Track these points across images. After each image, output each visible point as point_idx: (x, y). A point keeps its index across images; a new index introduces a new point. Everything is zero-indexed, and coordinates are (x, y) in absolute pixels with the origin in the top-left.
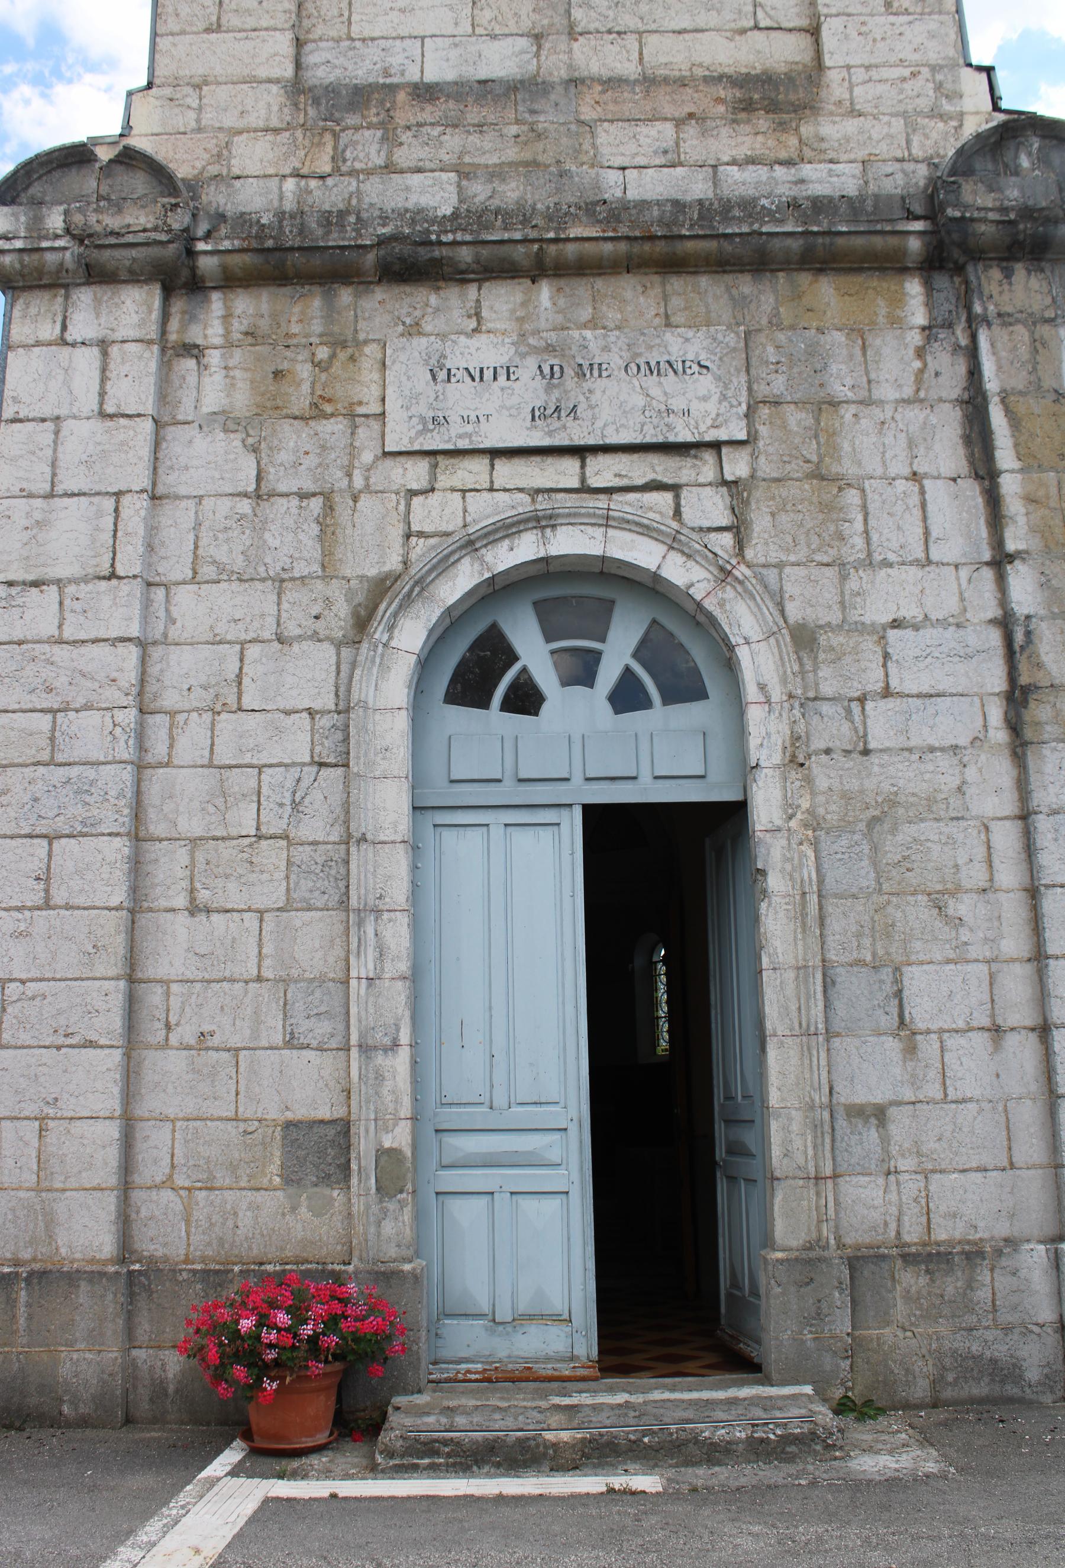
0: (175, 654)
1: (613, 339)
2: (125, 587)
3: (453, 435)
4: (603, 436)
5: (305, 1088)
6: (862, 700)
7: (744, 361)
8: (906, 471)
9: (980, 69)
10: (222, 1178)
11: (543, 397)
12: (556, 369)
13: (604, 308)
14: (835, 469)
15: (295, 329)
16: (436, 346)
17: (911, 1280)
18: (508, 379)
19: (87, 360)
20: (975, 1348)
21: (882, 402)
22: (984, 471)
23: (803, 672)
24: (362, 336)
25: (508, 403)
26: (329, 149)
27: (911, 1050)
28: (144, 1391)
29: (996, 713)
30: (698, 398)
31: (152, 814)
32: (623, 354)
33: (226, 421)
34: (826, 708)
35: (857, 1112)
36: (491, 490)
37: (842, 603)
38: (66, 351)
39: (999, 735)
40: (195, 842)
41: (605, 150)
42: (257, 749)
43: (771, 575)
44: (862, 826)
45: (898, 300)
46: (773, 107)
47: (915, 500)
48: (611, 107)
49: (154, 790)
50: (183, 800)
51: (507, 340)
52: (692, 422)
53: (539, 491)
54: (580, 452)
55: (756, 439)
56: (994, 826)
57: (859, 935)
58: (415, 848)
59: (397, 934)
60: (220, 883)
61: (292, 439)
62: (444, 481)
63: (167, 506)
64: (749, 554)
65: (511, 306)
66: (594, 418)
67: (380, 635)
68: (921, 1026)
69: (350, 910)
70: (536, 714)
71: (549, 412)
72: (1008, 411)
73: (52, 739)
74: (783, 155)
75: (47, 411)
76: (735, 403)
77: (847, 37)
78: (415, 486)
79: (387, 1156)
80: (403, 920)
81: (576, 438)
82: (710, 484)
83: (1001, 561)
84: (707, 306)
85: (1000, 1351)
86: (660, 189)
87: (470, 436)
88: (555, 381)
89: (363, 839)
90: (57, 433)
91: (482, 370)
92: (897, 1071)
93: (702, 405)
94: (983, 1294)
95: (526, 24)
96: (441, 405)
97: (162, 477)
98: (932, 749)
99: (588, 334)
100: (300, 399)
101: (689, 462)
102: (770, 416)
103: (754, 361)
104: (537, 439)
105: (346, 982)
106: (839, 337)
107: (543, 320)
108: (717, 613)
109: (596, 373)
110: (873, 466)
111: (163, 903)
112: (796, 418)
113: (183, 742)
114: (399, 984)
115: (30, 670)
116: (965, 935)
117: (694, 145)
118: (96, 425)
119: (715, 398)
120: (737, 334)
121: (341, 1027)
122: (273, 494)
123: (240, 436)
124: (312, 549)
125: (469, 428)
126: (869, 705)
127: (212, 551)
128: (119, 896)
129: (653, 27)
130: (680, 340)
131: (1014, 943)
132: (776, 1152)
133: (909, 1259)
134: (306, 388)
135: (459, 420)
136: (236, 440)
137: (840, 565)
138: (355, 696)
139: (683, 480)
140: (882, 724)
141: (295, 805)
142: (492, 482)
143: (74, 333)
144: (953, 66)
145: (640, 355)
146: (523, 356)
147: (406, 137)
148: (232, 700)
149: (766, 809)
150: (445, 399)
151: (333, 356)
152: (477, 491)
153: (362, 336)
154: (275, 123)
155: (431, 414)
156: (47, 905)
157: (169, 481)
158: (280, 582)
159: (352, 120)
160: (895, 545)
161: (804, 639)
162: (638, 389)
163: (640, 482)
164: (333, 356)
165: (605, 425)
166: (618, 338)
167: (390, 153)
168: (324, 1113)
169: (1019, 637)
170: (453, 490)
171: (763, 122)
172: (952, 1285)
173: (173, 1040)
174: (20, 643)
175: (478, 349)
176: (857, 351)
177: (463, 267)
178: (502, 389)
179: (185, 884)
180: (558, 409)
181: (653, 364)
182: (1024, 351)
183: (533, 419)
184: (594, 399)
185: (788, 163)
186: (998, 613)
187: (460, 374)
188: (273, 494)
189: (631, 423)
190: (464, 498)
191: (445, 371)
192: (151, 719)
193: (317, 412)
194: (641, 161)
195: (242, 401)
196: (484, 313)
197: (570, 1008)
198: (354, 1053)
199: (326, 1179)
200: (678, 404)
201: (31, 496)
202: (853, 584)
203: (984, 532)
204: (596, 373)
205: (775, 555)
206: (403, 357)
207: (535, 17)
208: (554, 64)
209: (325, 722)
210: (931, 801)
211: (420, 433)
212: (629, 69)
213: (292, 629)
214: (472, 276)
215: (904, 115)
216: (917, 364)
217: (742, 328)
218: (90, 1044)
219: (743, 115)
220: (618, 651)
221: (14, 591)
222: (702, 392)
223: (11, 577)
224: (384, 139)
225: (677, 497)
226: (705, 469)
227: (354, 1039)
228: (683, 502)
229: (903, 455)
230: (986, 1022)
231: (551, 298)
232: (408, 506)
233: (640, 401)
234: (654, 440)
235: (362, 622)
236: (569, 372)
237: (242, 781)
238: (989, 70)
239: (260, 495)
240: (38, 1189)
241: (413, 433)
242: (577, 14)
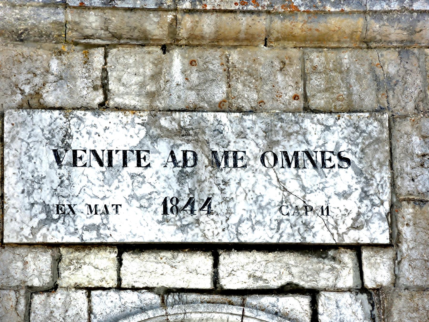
1: (248, 124)
3: (79, 227)
4: (238, 234)
7: (387, 154)
11: (176, 187)
12: (189, 155)
13: (240, 86)
16: (60, 123)
18: (139, 165)
25: (139, 192)
30: (337, 195)
32: (260, 141)
36: (119, 288)
51: (137, 120)
52: (331, 221)
53: (169, 291)
54: (214, 250)
55: (399, 242)
62: (68, 277)
65: (139, 79)
66: (229, 212)
71: (182, 204)
76: (377, 202)
78: (36, 283)
81: (209, 234)
82: (350, 290)
84: (349, 87)
87: (97, 228)
88: (189, 170)
91: (110, 153)
96: (66, 192)
99: (222, 116)
101: (327, 264)
102: (415, 215)
103: (398, 152)
104: (170, 234)
107: (174, 97)
109: (231, 162)
119: (356, 195)
120: (380, 121)
125: (97, 219)
130: (320, 128)
135: (86, 210)
139: (321, 284)
142: (119, 280)
145: (278, 143)
146: (154, 139)
150: (71, 184)
152: (103, 289)
155: (55, 201)
162: (275, 182)
163: (275, 284)
165: (241, 221)
166: (254, 123)
170: (78, 287)
175: (106, 129)
177: (89, 32)
178: (132, 176)
180: (191, 202)
181: (291, 154)
183: (165, 212)
184: (230, 190)
187: (86, 157)
189: (267, 220)
190: (89, 296)
191: (70, 153)
196: (112, 86)
200: (316, 200)
204: (231, 162)
206: (23, 134)
211: (43, 223)
214: (99, 42)
217: (386, 116)
222: (342, 188)
225: (314, 304)
226: (344, 273)
228: (320, 309)
231: (183, 72)
232: (29, 305)
233: (274, 195)
234: (291, 240)
236: (203, 160)
241: (35, 223)
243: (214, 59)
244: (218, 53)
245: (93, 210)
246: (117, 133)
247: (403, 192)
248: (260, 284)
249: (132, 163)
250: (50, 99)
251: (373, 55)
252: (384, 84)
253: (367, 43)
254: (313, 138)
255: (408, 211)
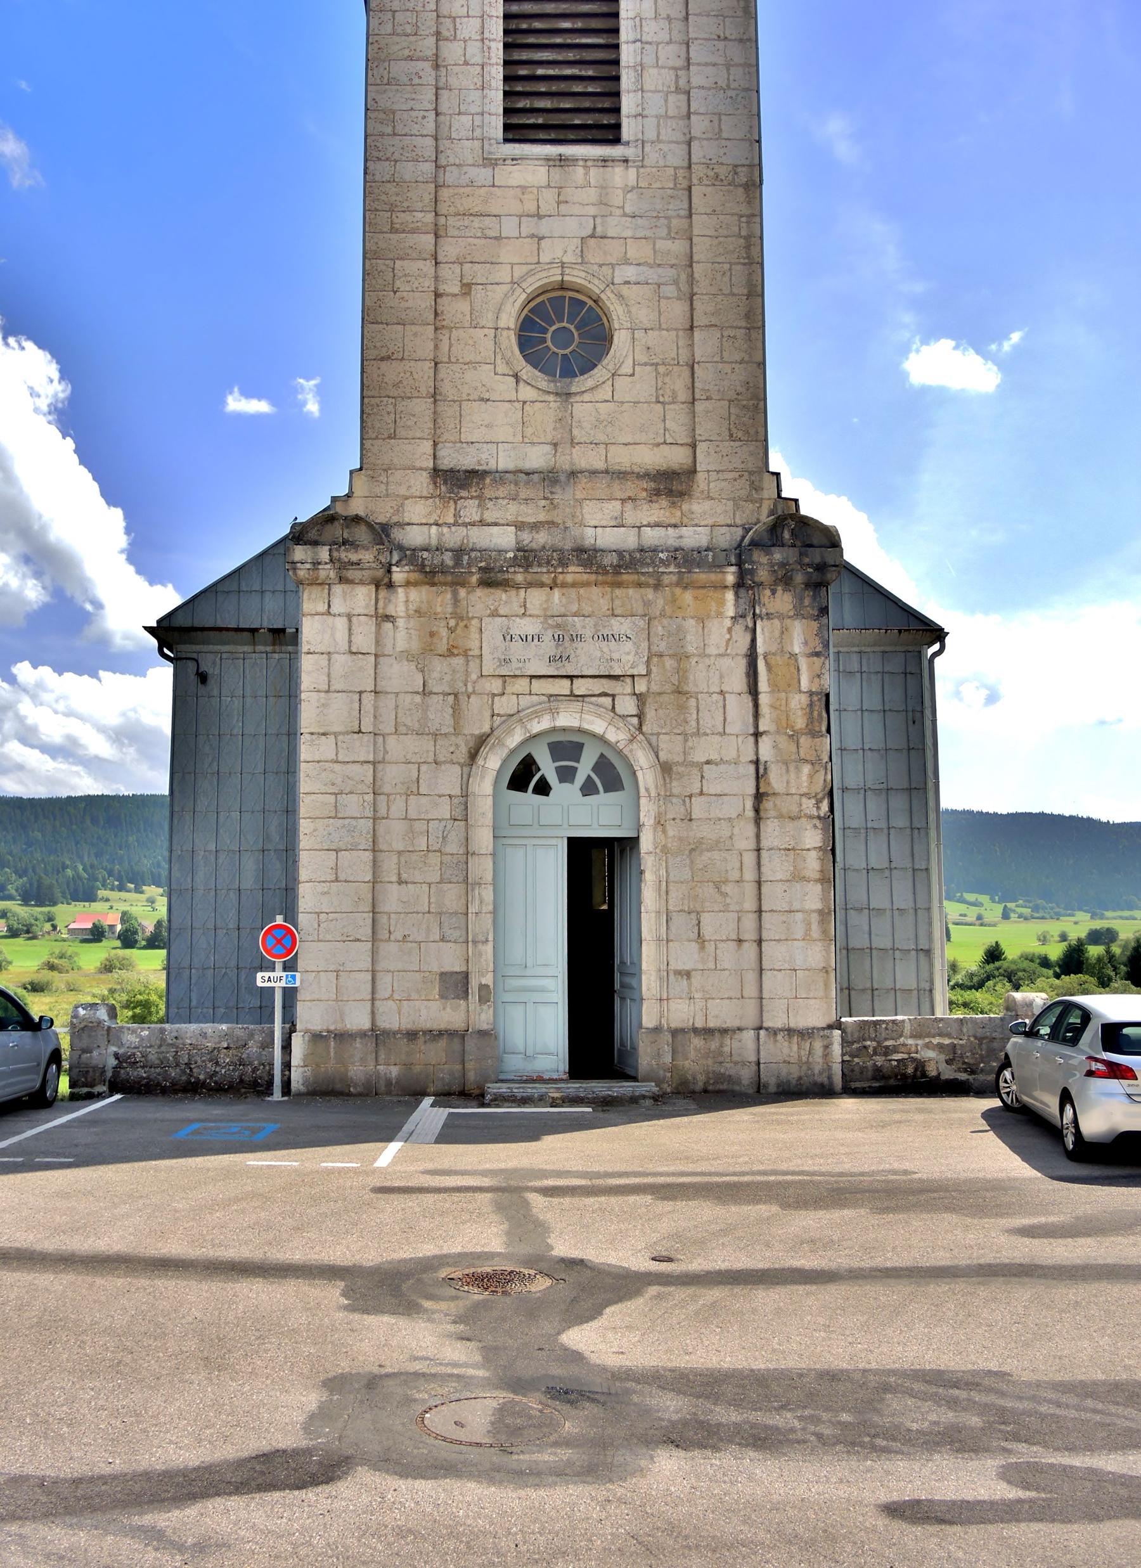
0: (389, 767)
2: (366, 738)
5: (450, 959)
6: (690, 796)
8: (718, 690)
9: (773, 473)
10: (414, 996)
14: (686, 688)
15: (439, 610)
17: (697, 1042)
19: (341, 624)
20: (722, 1071)
21: (710, 656)
22: (753, 691)
23: (665, 784)
24: (470, 615)
26: (452, 510)
27: (702, 948)
28: (382, 1083)
29: (749, 804)
31: (380, 840)
33: (408, 656)
34: (674, 800)
35: (678, 973)
37: (684, 752)
38: (331, 618)
39: (750, 813)
40: (400, 853)
41: (587, 516)
42: (427, 812)
43: (653, 739)
44: (687, 852)
45: (722, 602)
46: (670, 493)
47: (721, 704)
48: (590, 492)
49: (381, 830)
50: (394, 835)
53: (551, 696)
54: (571, 677)
56: (745, 854)
57: (683, 899)
58: (494, 855)
59: (488, 894)
60: (411, 871)
61: (438, 667)
62: (509, 689)
63: (382, 696)
64: (644, 728)
67: (481, 762)
68: (707, 938)
69: (467, 883)
70: (547, 795)
72: (767, 664)
73: (336, 807)
74: (673, 521)
75: (323, 649)
77: (709, 453)
79: (483, 988)
80: (491, 888)
83: (757, 735)
85: (732, 1072)
86: (612, 540)
89: (474, 853)
90: (329, 660)
92: (696, 956)
93: (627, 657)
94: (727, 1049)
95: (549, 439)
97: (379, 683)
98: (720, 819)
100: (442, 647)
105: (467, 914)
106: (692, 622)
108: (629, 755)
110: (703, 687)
111: (387, 879)
112: (669, 663)
113: (393, 808)
114: (489, 915)
115: (324, 775)
116: (728, 900)
117: (631, 517)
118: (348, 657)
121: (464, 933)
122: (431, 693)
123: (415, 663)
124: (449, 721)
125: (521, 665)
126: (693, 799)
127: (403, 719)
128: (369, 877)
129: (613, 441)
131: (750, 904)
132: (644, 988)
133: (695, 1030)
134: (445, 641)
136: (413, 666)
137: (685, 736)
138: (470, 790)
140: (698, 807)
141: (444, 838)
143: (334, 610)
144: (760, 472)
146: (546, 629)
147: (490, 504)
148: (415, 790)
149: (646, 843)
151: (457, 624)
153: (470, 615)
154: (425, 494)
156: (337, 880)
157: (383, 685)
158: (435, 736)
159: (464, 493)
160: (709, 725)
161: (666, 769)
163: (597, 692)
164: (457, 624)
167: (482, 514)
168: (457, 969)
169: (761, 771)
171: (664, 502)
172: (714, 1045)
173: (392, 938)
174: (318, 762)
176: (700, 629)
179: (396, 871)
182: (777, 633)
184: (578, 652)
185: (675, 526)
186: (754, 758)
187: (517, 638)
188: (431, 693)
192: (379, 798)
193: (450, 653)
194: (604, 523)
195: (415, 646)
197: (560, 924)
198: (470, 944)
199: (458, 997)
200: (615, 656)
201: (318, 691)
202: (690, 744)
203: (751, 720)
205: (656, 730)
206: (490, 628)
207: (554, 433)
208: (564, 462)
209: (456, 801)
210: (718, 842)
212: (600, 465)
213: (441, 758)
215: (734, 499)
216: (728, 636)
218: (358, 940)
219: (655, 498)
220: (585, 768)
221: (314, 737)
222: (627, 650)
223: (313, 731)
224: (479, 505)
225: (613, 700)
227: (470, 939)
229: (717, 682)
230: (735, 937)
233: (599, 654)
235: (473, 755)
237: (420, 826)
238: (778, 475)
239: (425, 692)
240: (336, 1000)
242: (575, 432)
243: (573, 592)
244: (574, 590)
245: (519, 661)
246: (528, 626)
247: (653, 652)
248: (590, 693)
249: (536, 640)
250: (501, 612)
251: (642, 590)
252: (647, 604)
253: (640, 585)
254: (615, 628)
255: (655, 659)
